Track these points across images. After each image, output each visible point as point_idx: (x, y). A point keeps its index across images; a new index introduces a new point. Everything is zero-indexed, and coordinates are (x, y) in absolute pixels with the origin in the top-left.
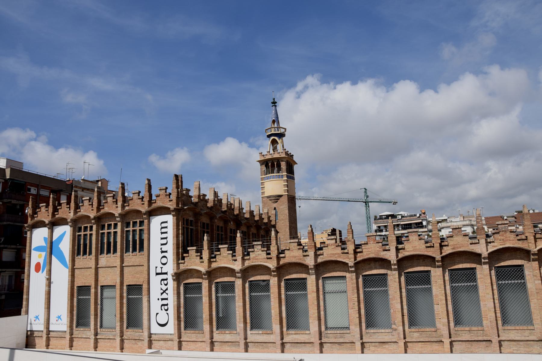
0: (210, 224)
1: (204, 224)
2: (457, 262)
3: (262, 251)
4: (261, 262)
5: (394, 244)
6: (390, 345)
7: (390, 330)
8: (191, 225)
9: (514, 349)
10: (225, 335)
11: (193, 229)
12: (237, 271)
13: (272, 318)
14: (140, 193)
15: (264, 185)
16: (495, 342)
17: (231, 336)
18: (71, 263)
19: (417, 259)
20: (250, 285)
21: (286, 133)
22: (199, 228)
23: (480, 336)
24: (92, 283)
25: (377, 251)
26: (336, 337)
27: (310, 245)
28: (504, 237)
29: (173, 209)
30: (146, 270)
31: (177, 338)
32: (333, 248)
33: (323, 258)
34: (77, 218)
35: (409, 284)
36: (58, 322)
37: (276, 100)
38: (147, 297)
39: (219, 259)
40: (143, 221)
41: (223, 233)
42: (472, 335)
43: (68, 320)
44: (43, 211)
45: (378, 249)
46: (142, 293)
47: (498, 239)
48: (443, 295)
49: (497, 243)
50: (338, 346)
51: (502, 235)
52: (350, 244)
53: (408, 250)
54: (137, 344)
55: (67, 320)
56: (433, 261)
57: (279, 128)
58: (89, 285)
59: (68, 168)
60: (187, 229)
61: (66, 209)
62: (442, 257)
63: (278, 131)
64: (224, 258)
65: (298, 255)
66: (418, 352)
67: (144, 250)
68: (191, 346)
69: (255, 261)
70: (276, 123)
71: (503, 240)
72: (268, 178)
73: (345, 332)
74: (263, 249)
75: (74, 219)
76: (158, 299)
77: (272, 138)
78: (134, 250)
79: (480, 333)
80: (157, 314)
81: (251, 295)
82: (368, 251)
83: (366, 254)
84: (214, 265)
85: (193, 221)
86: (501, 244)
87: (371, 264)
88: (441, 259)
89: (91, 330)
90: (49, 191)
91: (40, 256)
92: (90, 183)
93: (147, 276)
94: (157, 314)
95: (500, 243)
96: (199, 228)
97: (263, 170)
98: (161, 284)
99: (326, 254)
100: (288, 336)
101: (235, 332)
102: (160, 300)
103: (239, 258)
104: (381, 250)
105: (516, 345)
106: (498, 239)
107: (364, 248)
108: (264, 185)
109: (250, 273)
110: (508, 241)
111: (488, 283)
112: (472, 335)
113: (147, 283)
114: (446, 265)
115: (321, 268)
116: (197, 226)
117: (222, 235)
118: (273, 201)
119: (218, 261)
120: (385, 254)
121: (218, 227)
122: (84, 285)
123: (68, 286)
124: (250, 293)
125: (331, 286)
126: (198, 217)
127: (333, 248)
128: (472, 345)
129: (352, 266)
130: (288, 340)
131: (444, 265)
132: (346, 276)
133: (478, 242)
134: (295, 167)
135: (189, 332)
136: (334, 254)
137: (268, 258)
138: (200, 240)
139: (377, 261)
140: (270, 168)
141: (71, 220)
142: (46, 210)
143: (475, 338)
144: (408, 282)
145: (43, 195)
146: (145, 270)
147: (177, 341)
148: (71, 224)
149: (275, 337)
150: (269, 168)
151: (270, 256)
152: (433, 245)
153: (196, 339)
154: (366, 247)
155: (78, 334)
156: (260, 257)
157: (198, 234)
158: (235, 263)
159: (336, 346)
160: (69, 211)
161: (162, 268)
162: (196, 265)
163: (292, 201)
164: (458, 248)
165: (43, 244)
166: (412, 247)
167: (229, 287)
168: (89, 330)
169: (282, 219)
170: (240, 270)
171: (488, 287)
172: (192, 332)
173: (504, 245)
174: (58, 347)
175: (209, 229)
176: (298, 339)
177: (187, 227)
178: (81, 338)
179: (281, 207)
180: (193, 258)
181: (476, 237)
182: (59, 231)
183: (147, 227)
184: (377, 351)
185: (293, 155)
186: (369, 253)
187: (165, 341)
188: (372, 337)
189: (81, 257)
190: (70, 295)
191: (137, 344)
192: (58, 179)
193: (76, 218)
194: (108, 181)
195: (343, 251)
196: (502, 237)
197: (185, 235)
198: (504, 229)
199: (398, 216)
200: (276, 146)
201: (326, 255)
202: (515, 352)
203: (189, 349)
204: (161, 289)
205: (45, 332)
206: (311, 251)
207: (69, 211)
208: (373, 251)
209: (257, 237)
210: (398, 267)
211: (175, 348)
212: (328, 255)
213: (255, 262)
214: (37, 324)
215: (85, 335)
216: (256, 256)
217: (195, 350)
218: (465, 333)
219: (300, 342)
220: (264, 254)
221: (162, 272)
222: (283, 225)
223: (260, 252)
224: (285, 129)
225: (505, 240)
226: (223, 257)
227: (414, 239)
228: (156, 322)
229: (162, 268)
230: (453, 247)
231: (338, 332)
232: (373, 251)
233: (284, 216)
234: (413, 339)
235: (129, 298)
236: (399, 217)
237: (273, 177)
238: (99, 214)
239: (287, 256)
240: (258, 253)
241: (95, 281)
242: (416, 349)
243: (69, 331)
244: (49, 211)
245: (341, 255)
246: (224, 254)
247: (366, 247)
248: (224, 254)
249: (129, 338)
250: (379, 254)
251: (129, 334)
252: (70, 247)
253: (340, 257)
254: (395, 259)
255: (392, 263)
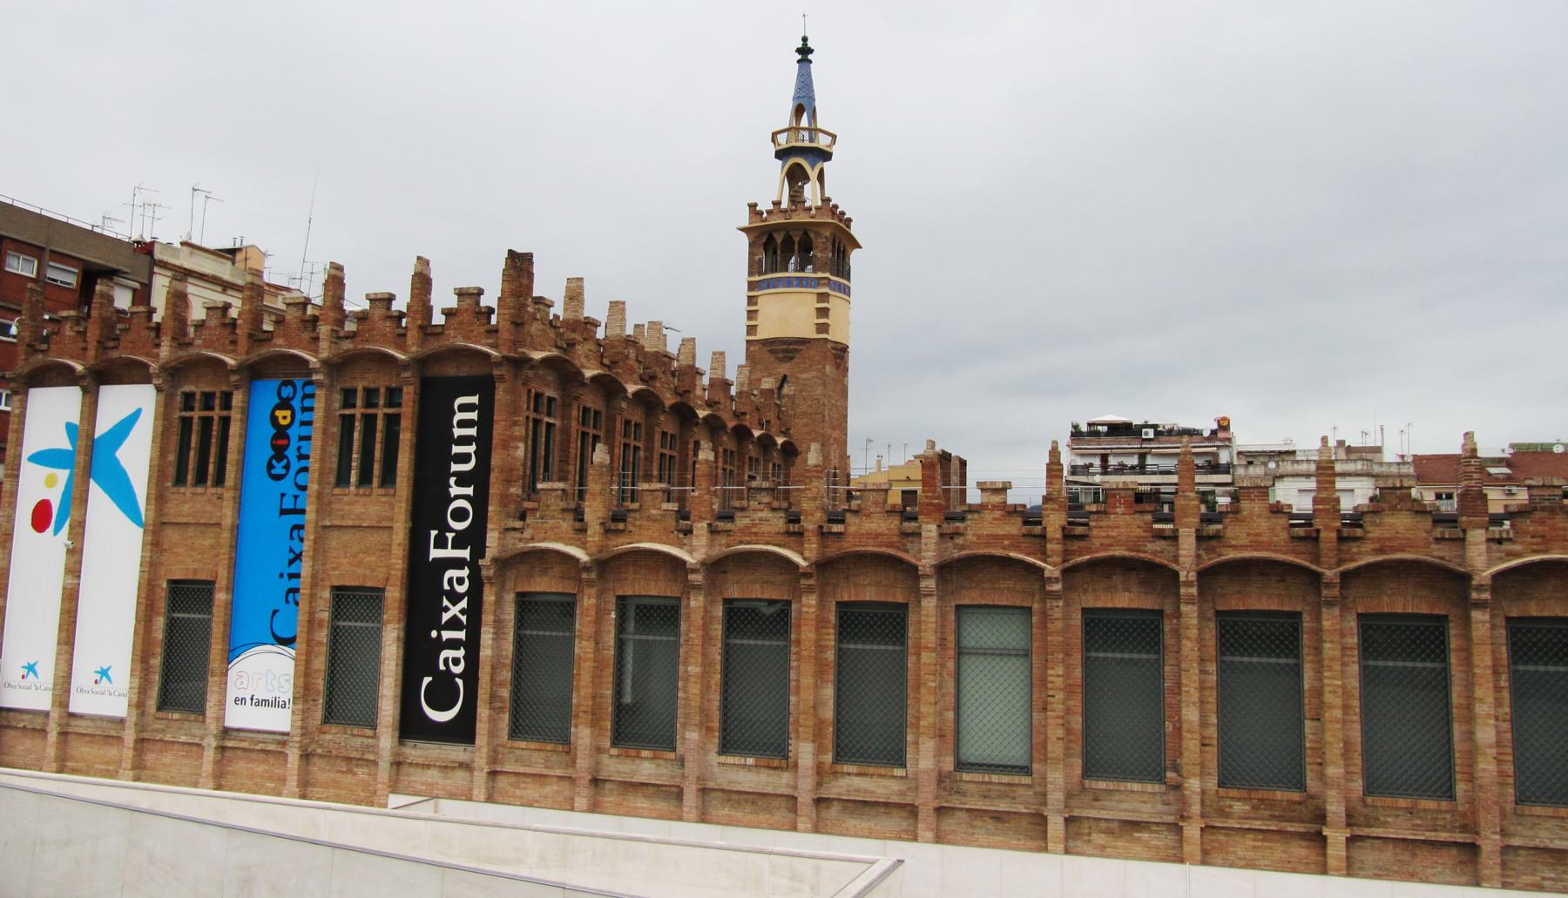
0: (604, 413)
1: (586, 410)
2: (1389, 592)
3: (774, 510)
4: (767, 543)
5: (1191, 519)
6: (1157, 832)
7: (1157, 788)
8: (549, 415)
9: (1545, 875)
10: (637, 762)
11: (554, 425)
12: (692, 567)
13: (791, 719)
14: (394, 302)
15: (756, 304)
16: (1492, 852)
17: (658, 765)
18: (153, 507)
19: (1262, 574)
20: (728, 614)
21: (835, 150)
22: (574, 424)
23: (1444, 828)
24: (220, 574)
25: (1136, 537)
26: (986, 793)
27: (928, 504)
28: (1546, 528)
29: (500, 360)
30: (399, 545)
31: (485, 760)
32: (997, 519)
33: (963, 547)
34: (181, 363)
35: (1228, 649)
36: (97, 688)
37: (810, 44)
38: (398, 629)
39: (634, 526)
40: (400, 390)
41: (640, 445)
42: (1418, 822)
43: (133, 685)
44: (68, 333)
45: (1139, 532)
46: (379, 615)
47: (1526, 533)
48: (1336, 692)
49: (1522, 543)
50: (990, 821)
51: (1542, 522)
52: (1052, 509)
53: (1233, 542)
54: (355, 774)
55: (131, 683)
56: (1311, 584)
57: (813, 131)
58: (209, 579)
59: (138, 201)
60: (537, 422)
61: (145, 332)
62: (1345, 576)
63: (811, 140)
64: (650, 524)
65: (886, 532)
66: (1243, 863)
67: (399, 480)
68: (525, 789)
69: (749, 539)
70: (805, 114)
71: (1542, 537)
72: (769, 284)
73: (1016, 779)
74: (776, 504)
75: (171, 368)
76: (281, 576)
77: (792, 161)
78: (365, 479)
79: (1445, 819)
80: (275, 612)
81: (728, 645)
82: (1107, 537)
83: (1101, 545)
84: (623, 545)
85: (554, 399)
86: (1535, 547)
87: (1114, 577)
88: (1338, 581)
89: (208, 720)
90: (76, 270)
91: (51, 482)
92: (208, 255)
93: (400, 561)
94: (275, 612)
95: (1532, 544)
96: (574, 424)
97: (757, 258)
98: (292, 538)
99: (974, 535)
100: (838, 778)
101: (671, 755)
102: (286, 577)
103: (699, 525)
104: (1147, 537)
105: (1552, 864)
106: (1526, 533)
107: (1095, 527)
108: (756, 304)
109: (730, 576)
110: (1557, 541)
111: (1485, 667)
112: (1418, 822)
113: (399, 583)
114: (1351, 599)
115: (954, 577)
116: (565, 417)
117: (636, 448)
118: (781, 355)
119: (630, 532)
120: (1158, 549)
121: (627, 422)
122: (191, 577)
123: (140, 577)
124: (728, 637)
125: (981, 633)
126: (574, 390)
127: (997, 519)
128: (1414, 855)
129: (1056, 578)
130: (836, 790)
131: (1347, 598)
132: (1031, 608)
133: (1462, 536)
134: (855, 257)
135: (523, 744)
136: (997, 535)
137: (788, 533)
138: (572, 462)
139: (1133, 569)
140: (779, 253)
141: (163, 368)
142: (78, 332)
143: (1428, 834)
144: (1228, 641)
145: (56, 281)
146: (397, 542)
147: (482, 769)
148: (160, 381)
149: (806, 789)
150: (775, 252)
151: (797, 526)
152: (1314, 535)
153: (546, 767)
154: (1101, 524)
155: (163, 730)
156: (764, 528)
157: (569, 442)
158: (685, 541)
159: (984, 821)
160: (156, 341)
161: (296, 497)
162: (559, 539)
163: (838, 361)
164: (1394, 550)
165: (65, 444)
166: (1249, 534)
167: (664, 615)
168: (201, 718)
169: (805, 413)
170: (703, 563)
171: (1484, 680)
172: (533, 745)
173: (1545, 552)
174: (97, 766)
175: (600, 429)
176: (866, 791)
177: (538, 417)
178: (173, 742)
179: (805, 376)
180: (553, 517)
181: (1456, 521)
182: (119, 401)
183: (410, 409)
184: (1115, 847)
185: (850, 220)
186: (1108, 541)
187: (446, 767)
188: (1099, 803)
189: (188, 490)
190: (143, 607)
191: (355, 774)
192: (105, 233)
193: (179, 366)
194: (265, 255)
195: (1025, 529)
196: (1540, 528)
197: (530, 443)
198: (1547, 503)
199: (1144, 430)
200: (802, 187)
201: (974, 539)
202: (1547, 883)
203: (522, 797)
204: (291, 550)
205: (55, 715)
206: (928, 523)
207: (156, 341)
208: (1123, 538)
209: (736, 463)
210: (1201, 592)
211: (475, 792)
212: (979, 537)
213: (749, 543)
214: (29, 688)
215: (186, 735)
216: (754, 525)
217: (537, 801)
218: (1397, 816)
219: (873, 800)
220: (777, 522)
221: (298, 507)
222: (805, 429)
223: (766, 514)
224: (834, 137)
225: (1548, 537)
226: (649, 518)
227: (1256, 509)
228: (269, 627)
229: (296, 497)
230: (1377, 546)
231: (995, 778)
232: (1123, 538)
233: (809, 402)
234: (1230, 821)
235: (338, 627)
236: (1147, 434)
237: (788, 282)
238: (254, 357)
239: (852, 529)
240: (760, 514)
241: (229, 567)
242: (1235, 852)
243: (134, 719)
244: (88, 335)
245: (1022, 540)
246: (654, 512)
247: (1101, 524)
248: (654, 512)
249: (330, 752)
250: (1142, 548)
251: (330, 740)
252: (151, 455)
253: (1017, 548)
254: (1194, 567)
255: (1182, 579)
